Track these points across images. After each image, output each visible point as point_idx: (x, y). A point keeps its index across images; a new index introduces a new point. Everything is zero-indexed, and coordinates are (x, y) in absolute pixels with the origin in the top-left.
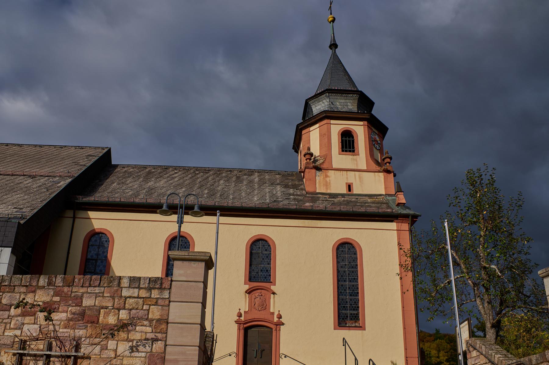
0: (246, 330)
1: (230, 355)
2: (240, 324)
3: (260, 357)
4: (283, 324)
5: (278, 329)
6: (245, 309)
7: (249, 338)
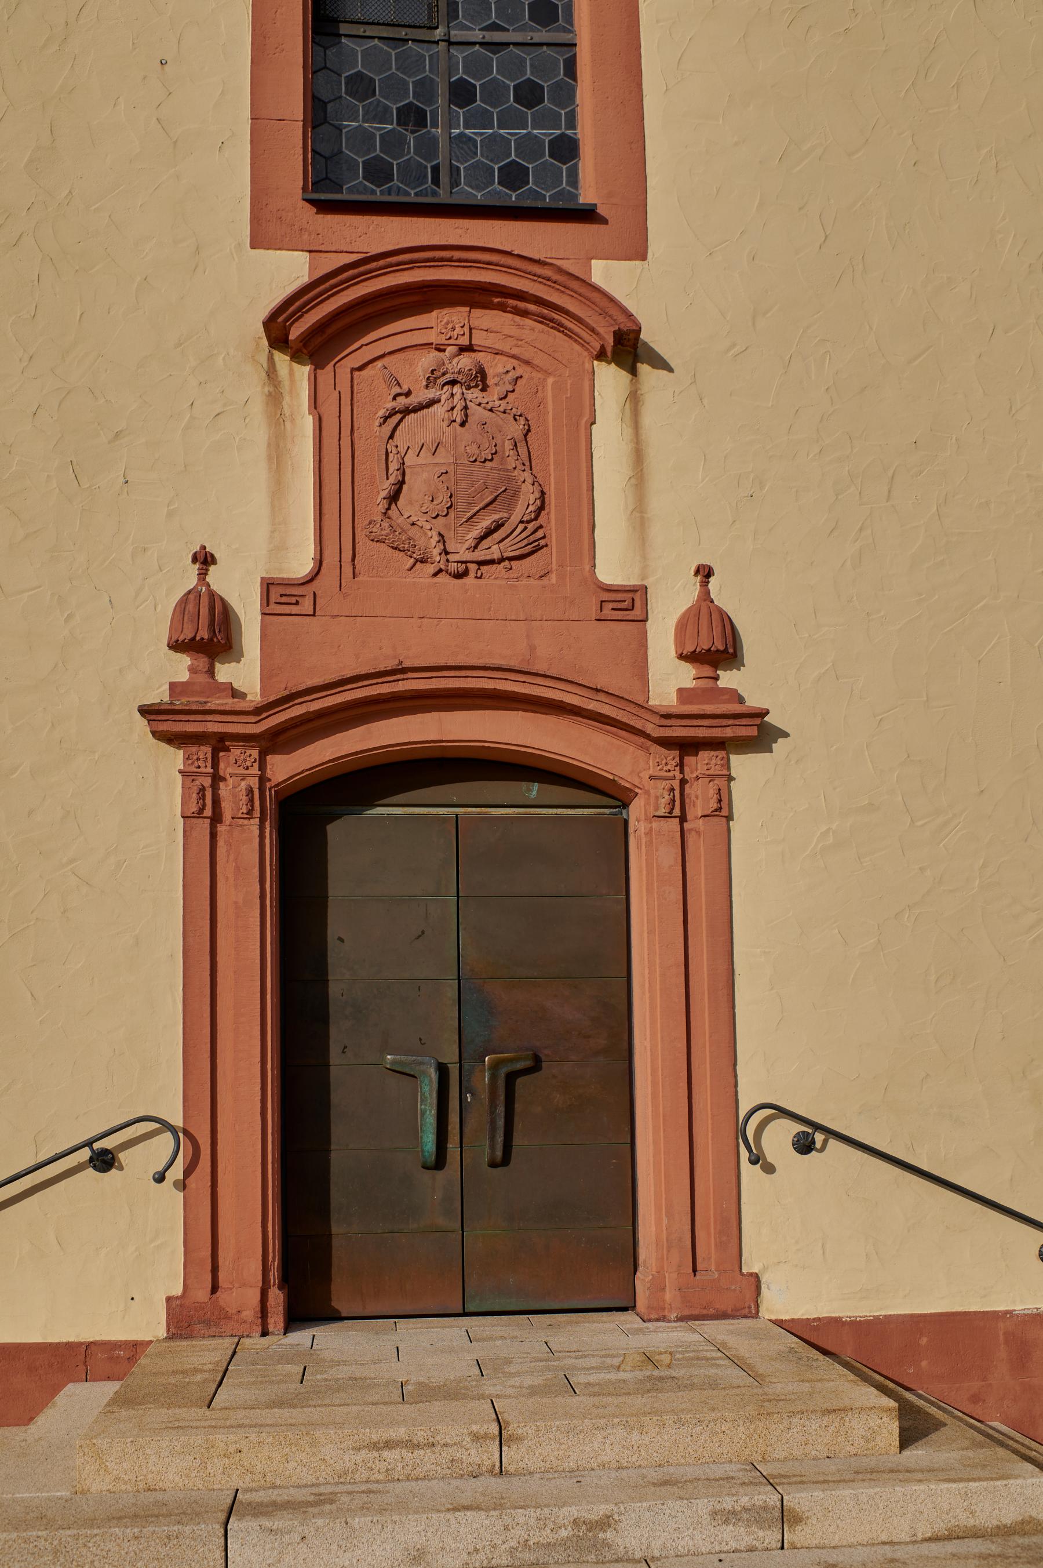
0: (302, 820)
1: (104, 1161)
2: (220, 743)
3: (483, 1150)
4: (758, 733)
5: (701, 798)
6: (279, 548)
7: (338, 924)
